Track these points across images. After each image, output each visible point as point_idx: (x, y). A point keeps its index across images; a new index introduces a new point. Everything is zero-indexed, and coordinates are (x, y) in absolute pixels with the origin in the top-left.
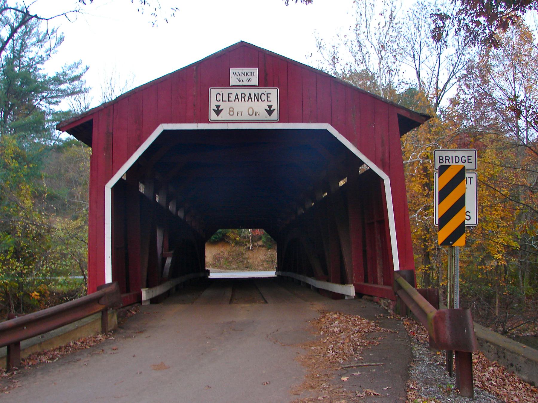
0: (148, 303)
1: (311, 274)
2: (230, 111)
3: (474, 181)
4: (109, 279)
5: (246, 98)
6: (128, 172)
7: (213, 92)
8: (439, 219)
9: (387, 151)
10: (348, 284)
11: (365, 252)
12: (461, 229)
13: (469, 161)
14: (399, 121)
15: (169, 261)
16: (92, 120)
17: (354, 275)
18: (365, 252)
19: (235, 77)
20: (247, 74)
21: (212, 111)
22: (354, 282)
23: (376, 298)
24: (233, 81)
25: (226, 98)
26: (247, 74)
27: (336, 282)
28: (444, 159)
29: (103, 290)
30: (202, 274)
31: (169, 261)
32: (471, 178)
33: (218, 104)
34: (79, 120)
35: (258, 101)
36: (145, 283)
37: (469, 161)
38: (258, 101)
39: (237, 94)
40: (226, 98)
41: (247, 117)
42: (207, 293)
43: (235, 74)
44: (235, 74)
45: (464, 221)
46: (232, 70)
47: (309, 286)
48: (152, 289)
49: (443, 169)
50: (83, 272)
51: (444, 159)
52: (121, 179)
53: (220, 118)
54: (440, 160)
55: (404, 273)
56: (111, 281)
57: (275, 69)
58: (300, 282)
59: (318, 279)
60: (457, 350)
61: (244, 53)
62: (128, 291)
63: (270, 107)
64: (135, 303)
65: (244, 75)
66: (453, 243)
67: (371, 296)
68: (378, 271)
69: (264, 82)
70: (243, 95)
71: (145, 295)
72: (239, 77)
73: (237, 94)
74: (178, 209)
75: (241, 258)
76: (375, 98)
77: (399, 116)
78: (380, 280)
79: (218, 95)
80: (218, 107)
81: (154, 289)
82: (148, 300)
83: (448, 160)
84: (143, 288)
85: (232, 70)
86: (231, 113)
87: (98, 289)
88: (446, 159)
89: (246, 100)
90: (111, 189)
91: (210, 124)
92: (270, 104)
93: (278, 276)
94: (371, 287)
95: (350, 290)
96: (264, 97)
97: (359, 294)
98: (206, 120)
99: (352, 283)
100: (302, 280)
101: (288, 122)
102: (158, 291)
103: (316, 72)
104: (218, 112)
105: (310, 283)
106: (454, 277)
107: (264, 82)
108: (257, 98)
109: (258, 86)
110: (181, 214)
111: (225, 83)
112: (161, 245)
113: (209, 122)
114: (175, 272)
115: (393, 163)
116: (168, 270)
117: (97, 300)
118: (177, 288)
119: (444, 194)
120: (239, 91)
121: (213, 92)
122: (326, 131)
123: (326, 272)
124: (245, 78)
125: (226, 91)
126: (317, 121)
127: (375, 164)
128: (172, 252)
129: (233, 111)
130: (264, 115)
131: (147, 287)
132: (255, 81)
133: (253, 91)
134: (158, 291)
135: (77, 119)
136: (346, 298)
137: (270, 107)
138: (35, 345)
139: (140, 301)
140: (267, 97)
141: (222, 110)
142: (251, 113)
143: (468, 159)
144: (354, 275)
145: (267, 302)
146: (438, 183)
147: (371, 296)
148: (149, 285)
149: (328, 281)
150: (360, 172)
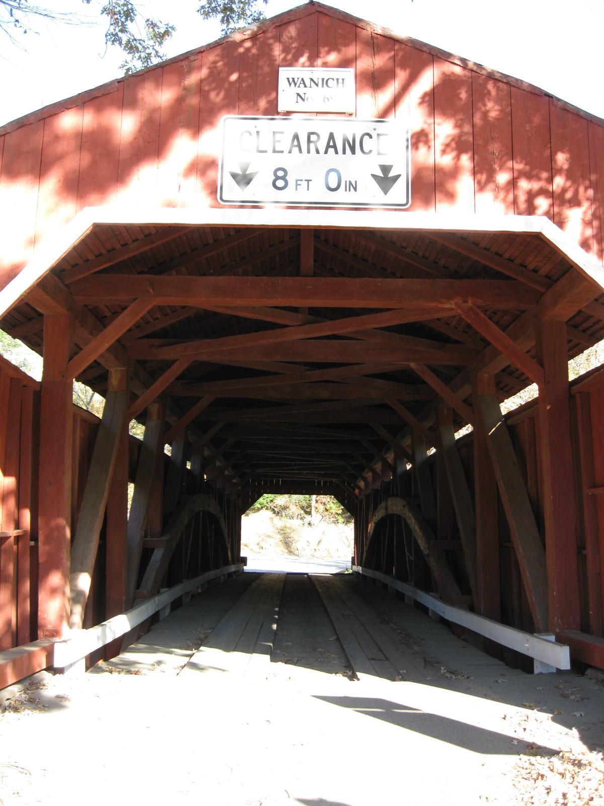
1: (428, 586)
2: (277, 178)
5: (322, 146)
19: (294, 90)
22: (557, 630)
24: (286, 98)
27: (490, 615)
30: (233, 568)
35: (353, 152)
38: (353, 152)
41: (319, 194)
43: (292, 82)
44: (292, 82)
47: (424, 609)
53: (248, 193)
59: (446, 599)
70: (313, 138)
72: (301, 90)
86: (280, 183)
89: (322, 149)
97: (579, 665)
103: (508, 83)
118: (176, 605)
123: (464, 587)
129: (283, 178)
130: (370, 192)
136: (537, 670)
137: (385, 169)
142: (333, 185)
150: (572, 377)
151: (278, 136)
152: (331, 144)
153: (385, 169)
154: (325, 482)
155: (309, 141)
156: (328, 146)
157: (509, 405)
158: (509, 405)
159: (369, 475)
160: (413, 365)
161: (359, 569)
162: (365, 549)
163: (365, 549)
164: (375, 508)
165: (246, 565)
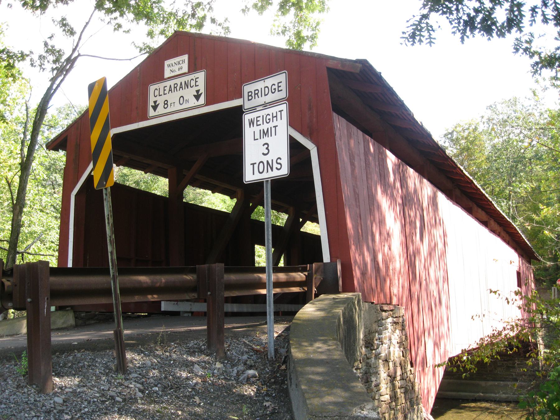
2: (165, 104)
5: (178, 88)
13: (280, 89)
20: (179, 63)
21: (151, 107)
26: (179, 63)
28: (253, 95)
33: (155, 99)
37: (280, 89)
41: (178, 107)
50: (550, 128)
51: (253, 95)
54: (249, 96)
56: (205, 304)
72: (171, 68)
83: (257, 94)
88: (255, 94)
92: (197, 88)
96: (193, 83)
104: (155, 108)
107: (193, 68)
108: (187, 85)
124: (176, 68)
125: (161, 85)
130: (193, 102)
153: (198, 91)
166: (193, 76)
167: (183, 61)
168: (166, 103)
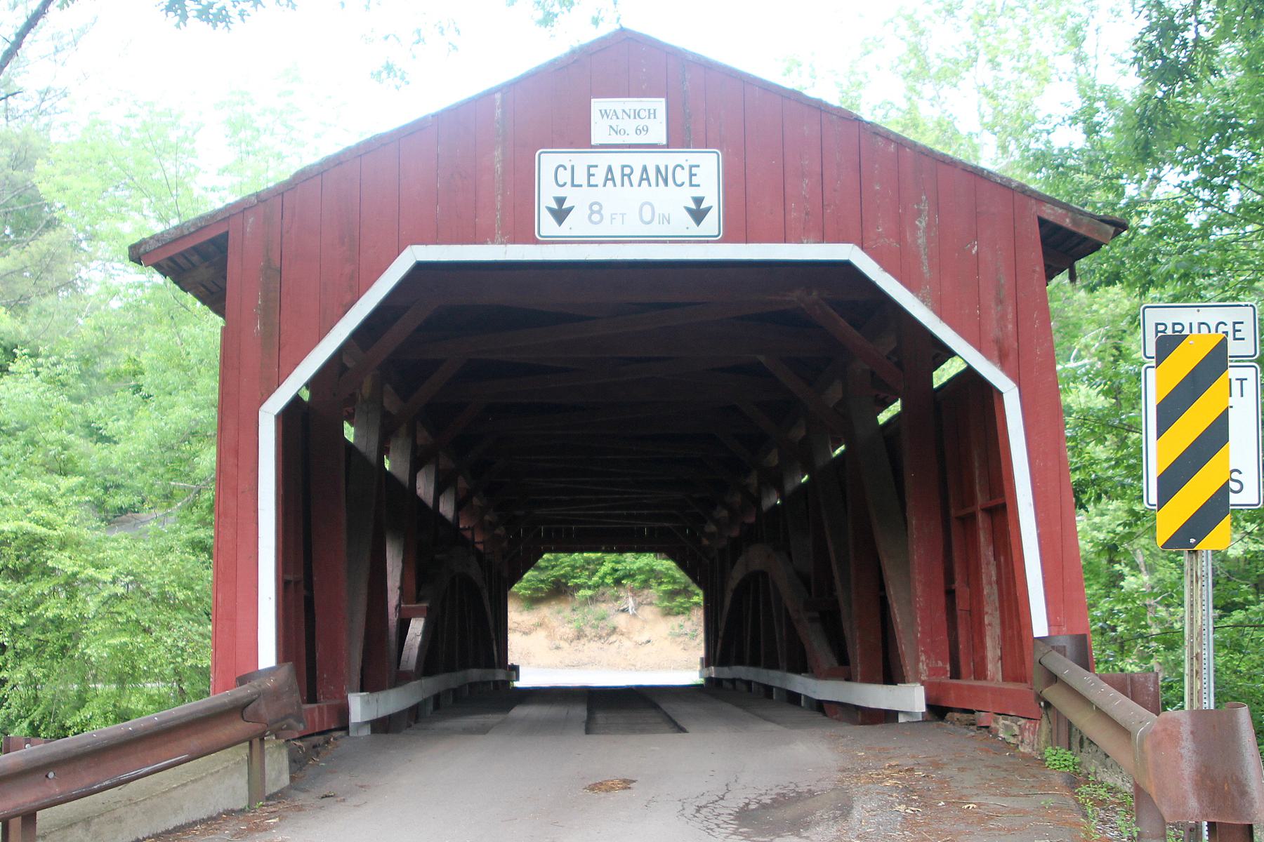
0: (366, 731)
1: (801, 665)
2: (592, 212)
3: (1250, 386)
4: (267, 656)
5: (636, 178)
6: (311, 384)
7: (548, 162)
8: (1159, 478)
9: (1010, 316)
10: (903, 681)
11: (950, 594)
12: (1216, 509)
13: (1238, 335)
14: (1044, 240)
15: (417, 627)
16: (227, 232)
17: (923, 658)
18: (950, 594)
20: (637, 114)
23: (983, 718)
24: (599, 134)
25: (581, 178)
26: (637, 114)
29: (255, 683)
30: (500, 675)
31: (417, 627)
32: (1242, 380)
33: (561, 193)
34: (191, 234)
35: (666, 184)
36: (356, 679)
37: (1238, 335)
38: (666, 184)
39: (610, 169)
40: (581, 178)
42: (519, 712)
43: (604, 114)
44: (604, 114)
45: (1227, 483)
46: (597, 105)
47: (794, 699)
48: (376, 695)
49: (1167, 344)
52: (297, 399)
53: (565, 229)
55: (1063, 640)
57: (710, 105)
58: (768, 690)
60: (1212, 820)
61: (627, 62)
62: (312, 698)
63: (698, 201)
64: (335, 730)
65: (629, 117)
66: (1196, 543)
67: (972, 712)
68: (989, 643)
69: (681, 135)
71: (360, 707)
72: (614, 122)
73: (610, 169)
74: (439, 491)
75: (608, 627)
76: (976, 174)
77: (1043, 222)
78: (994, 668)
79: (561, 169)
80: (560, 201)
81: (381, 695)
82: (366, 723)
84: (353, 691)
85: (597, 105)
87: (242, 680)
90: (278, 417)
91: (539, 247)
92: (697, 193)
93: (709, 680)
94: (971, 688)
95: (910, 698)
96: (682, 176)
97: (937, 711)
98: (527, 235)
99: (917, 679)
100: (777, 683)
101: (747, 242)
102: (392, 701)
103: (819, 108)
104: (560, 214)
105: (798, 689)
106: (1200, 634)
108: (663, 177)
109: (668, 146)
110: (447, 508)
111: (576, 135)
112: (398, 584)
113: (537, 242)
114: (430, 662)
115: (1031, 355)
116: (415, 652)
117: (239, 709)
119: (1170, 412)
120: (617, 160)
121: (548, 162)
122: (847, 266)
124: (629, 125)
125: (579, 160)
126: (823, 239)
127: (980, 350)
128: (425, 605)
129: (599, 212)
130: (685, 225)
131: (362, 691)
132: (658, 133)
133: (652, 160)
134: (392, 701)
135: (186, 232)
136: (902, 719)
137: (698, 201)
138: (72, 824)
139: (343, 723)
140: (691, 175)
141: (569, 210)
143: (1235, 331)
144: (923, 658)
145: (682, 730)
146: (1156, 385)
147: (972, 712)
148: (366, 685)
149: (849, 678)
150: (935, 386)
151: (592, 171)
152: (644, 176)
154: (651, 530)
155: (623, 175)
156: (642, 179)
157: (883, 418)
158: (883, 418)
159: (723, 513)
160: (762, 358)
161: (713, 672)
162: (721, 634)
163: (721, 634)
164: (733, 563)
165: (518, 679)
166: (669, 159)
167: (652, 114)
168: (595, 209)
